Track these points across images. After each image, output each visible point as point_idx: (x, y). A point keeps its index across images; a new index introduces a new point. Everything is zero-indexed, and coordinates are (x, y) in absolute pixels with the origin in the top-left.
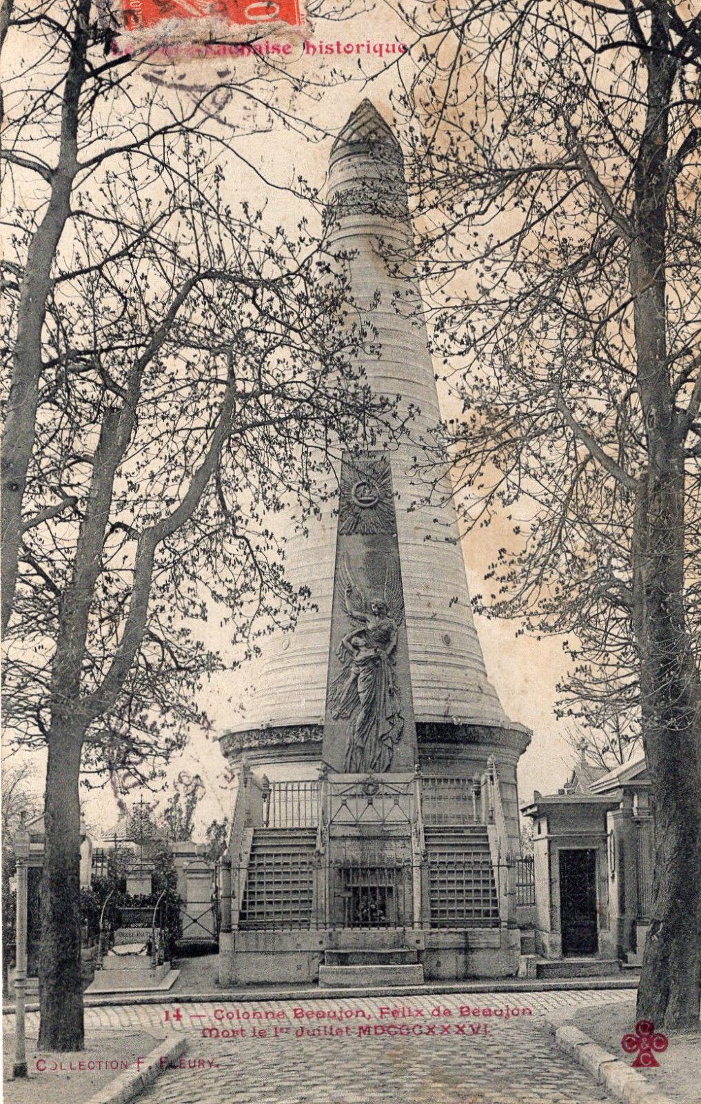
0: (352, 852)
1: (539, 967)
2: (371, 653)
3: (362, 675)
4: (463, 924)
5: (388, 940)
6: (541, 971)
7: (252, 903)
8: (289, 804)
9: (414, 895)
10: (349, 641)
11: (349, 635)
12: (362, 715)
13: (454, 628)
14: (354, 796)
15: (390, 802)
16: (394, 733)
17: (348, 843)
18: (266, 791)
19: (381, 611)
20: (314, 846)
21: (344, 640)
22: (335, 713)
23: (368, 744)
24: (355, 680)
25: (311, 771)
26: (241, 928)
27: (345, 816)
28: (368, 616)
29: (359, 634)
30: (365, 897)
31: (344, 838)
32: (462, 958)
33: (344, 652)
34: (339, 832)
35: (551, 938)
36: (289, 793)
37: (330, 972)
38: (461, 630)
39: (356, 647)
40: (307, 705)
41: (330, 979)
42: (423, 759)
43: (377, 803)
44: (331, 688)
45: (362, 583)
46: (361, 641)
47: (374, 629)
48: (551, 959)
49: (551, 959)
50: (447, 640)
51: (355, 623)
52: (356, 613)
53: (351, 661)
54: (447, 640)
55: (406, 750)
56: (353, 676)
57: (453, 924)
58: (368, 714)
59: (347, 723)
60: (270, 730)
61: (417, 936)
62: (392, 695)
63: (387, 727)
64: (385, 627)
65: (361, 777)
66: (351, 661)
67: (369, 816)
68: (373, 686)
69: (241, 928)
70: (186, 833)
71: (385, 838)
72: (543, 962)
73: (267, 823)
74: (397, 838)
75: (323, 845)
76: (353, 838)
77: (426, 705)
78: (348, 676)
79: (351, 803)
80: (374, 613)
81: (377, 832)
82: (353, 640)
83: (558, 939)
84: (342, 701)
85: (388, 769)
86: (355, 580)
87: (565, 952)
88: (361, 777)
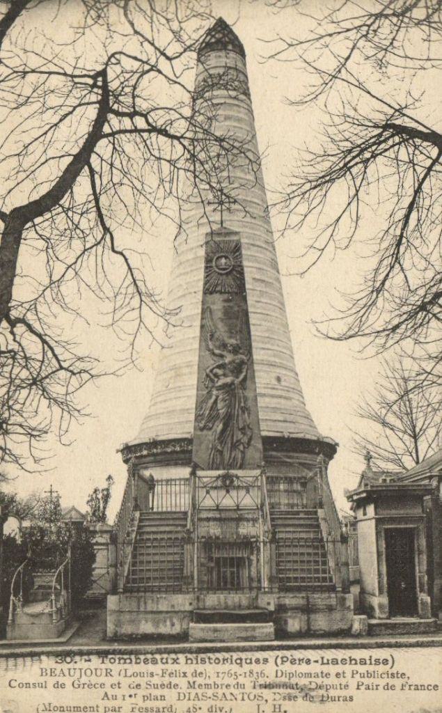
0: (214, 530)
1: (370, 626)
2: (229, 380)
3: (221, 397)
4: (306, 589)
5: (245, 602)
6: (371, 631)
7: (142, 562)
8: (169, 496)
9: (262, 563)
10: (211, 371)
11: (211, 368)
12: (221, 426)
13: (284, 372)
14: (216, 488)
15: (242, 493)
16: (245, 439)
17: (211, 523)
18: (151, 484)
19: (235, 350)
20: (186, 526)
21: (208, 371)
22: (201, 425)
23: (226, 448)
24: (215, 402)
25: (185, 472)
26: (126, 590)
27: (208, 502)
28: (225, 353)
29: (219, 367)
30: (226, 563)
31: (208, 519)
32: (305, 617)
33: (208, 378)
34: (204, 515)
35: (379, 601)
36: (173, 486)
37: (197, 629)
38: (288, 373)
39: (216, 375)
40: (178, 421)
41: (200, 635)
42: (269, 461)
43: (234, 493)
44: (200, 404)
45: (222, 330)
46: (220, 372)
47: (230, 363)
48: (380, 618)
49: (380, 618)
50: (279, 379)
51: (215, 358)
52: (217, 352)
53: (213, 387)
54: (279, 379)
55: (255, 452)
56: (214, 398)
57: (299, 589)
58: (226, 426)
59: (210, 433)
60: (155, 444)
61: (269, 602)
62: (243, 412)
63: (240, 436)
64: (237, 361)
65: (221, 472)
66: (213, 387)
67: (228, 501)
68: (230, 406)
69: (126, 590)
70: (103, 518)
71: (239, 520)
72: (374, 622)
73: (152, 508)
74: (248, 520)
75: (193, 525)
76: (215, 519)
77: (270, 422)
78: (211, 397)
79: (214, 493)
80: (230, 351)
81: (235, 515)
82: (215, 371)
83: (385, 600)
84: (205, 418)
85: (241, 467)
86: (216, 328)
87: (392, 614)
88: (221, 472)
